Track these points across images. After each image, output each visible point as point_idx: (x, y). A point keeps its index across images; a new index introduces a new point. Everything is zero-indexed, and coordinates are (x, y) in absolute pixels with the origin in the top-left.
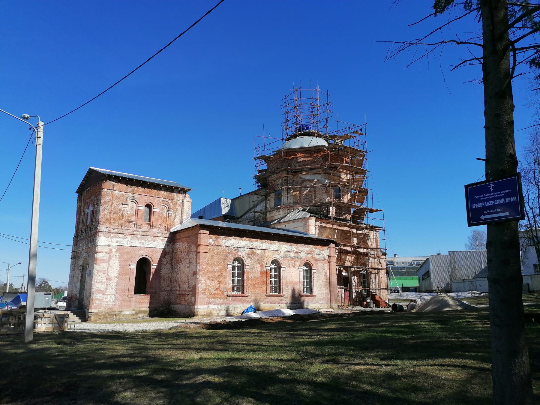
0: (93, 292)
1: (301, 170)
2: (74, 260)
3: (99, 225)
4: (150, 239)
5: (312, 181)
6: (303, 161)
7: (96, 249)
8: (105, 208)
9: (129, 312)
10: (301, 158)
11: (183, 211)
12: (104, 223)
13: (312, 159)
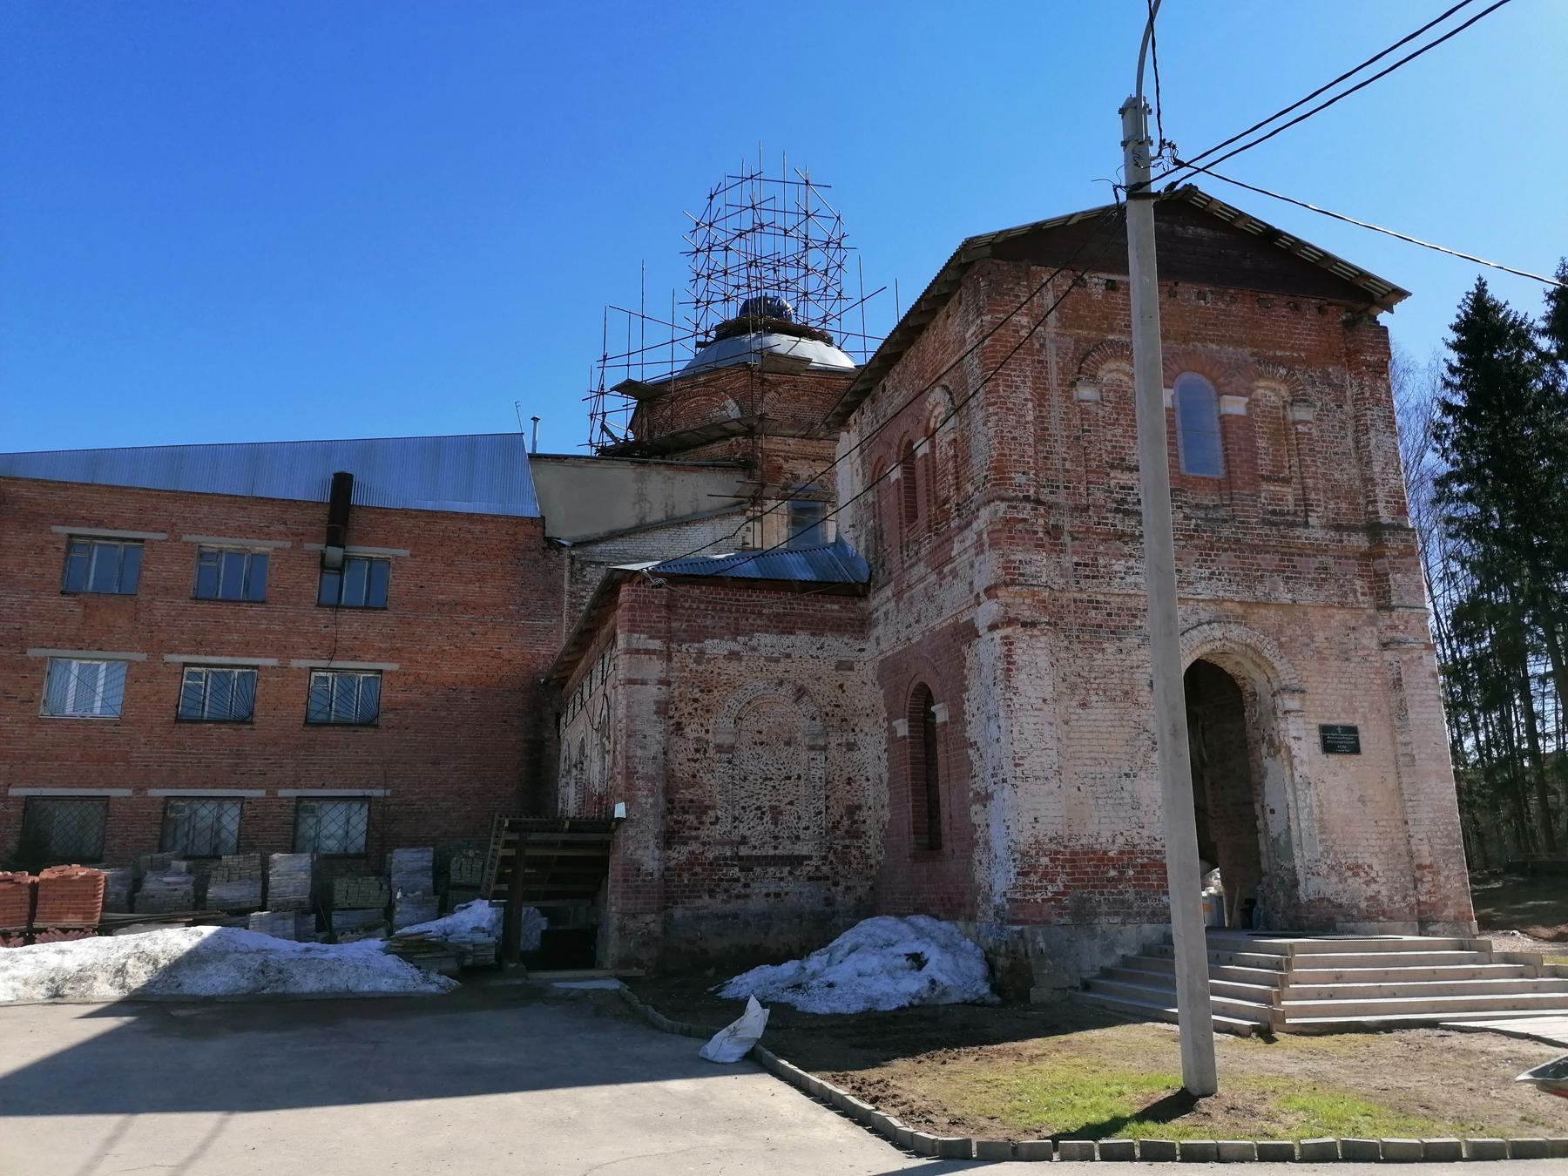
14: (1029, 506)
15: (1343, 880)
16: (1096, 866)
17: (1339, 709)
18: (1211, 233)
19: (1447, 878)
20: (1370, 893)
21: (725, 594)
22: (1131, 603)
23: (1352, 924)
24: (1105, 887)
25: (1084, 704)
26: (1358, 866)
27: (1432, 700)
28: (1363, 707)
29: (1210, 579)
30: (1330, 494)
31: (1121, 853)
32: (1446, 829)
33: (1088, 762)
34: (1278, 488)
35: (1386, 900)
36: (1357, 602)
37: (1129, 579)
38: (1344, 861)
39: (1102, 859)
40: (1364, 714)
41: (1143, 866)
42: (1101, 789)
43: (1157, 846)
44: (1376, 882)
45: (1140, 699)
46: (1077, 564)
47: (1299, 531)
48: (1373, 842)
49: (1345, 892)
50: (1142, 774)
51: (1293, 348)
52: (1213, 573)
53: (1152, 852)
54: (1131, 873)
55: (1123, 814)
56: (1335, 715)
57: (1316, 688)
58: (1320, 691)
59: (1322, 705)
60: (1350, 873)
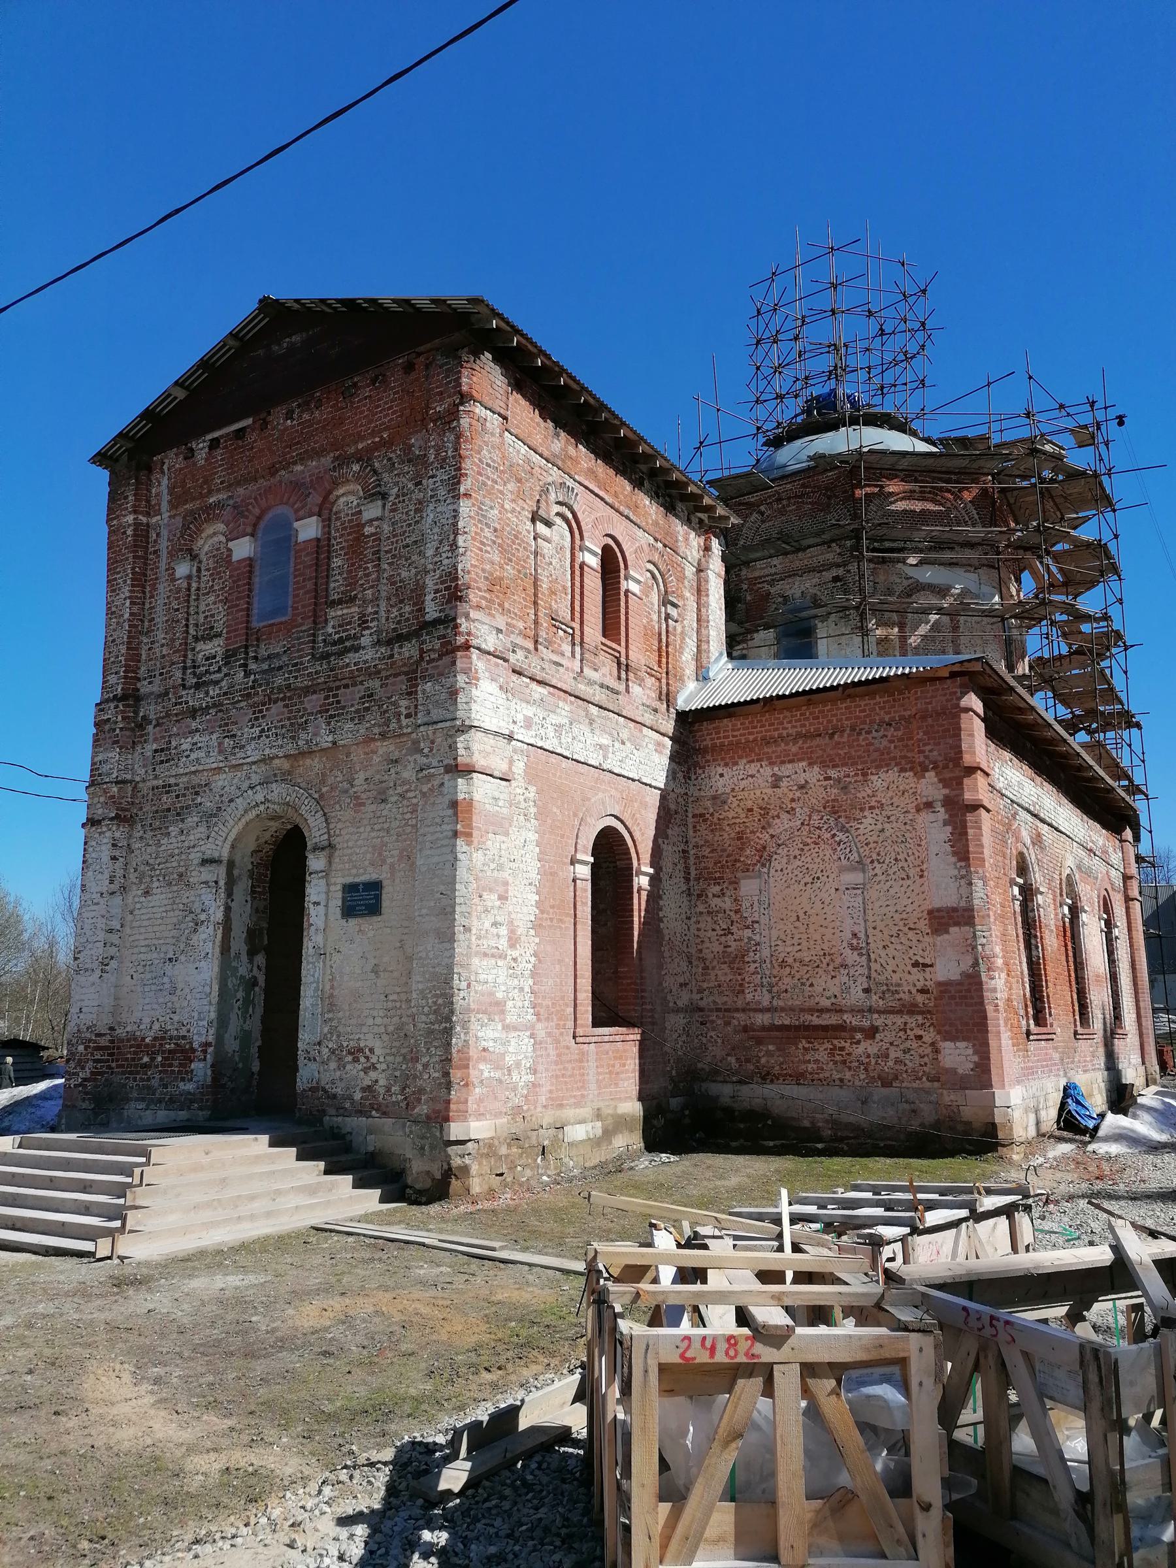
0: (468, 1010)
1: (902, 544)
2: (114, 832)
3: (462, 607)
4: (625, 734)
5: (942, 591)
6: (905, 511)
7: (461, 751)
8: (482, 518)
9: (583, 1125)
10: (897, 501)
11: (704, 617)
12: (484, 603)
13: (937, 508)
14: (112, 705)
15: (342, 1066)
16: (135, 1053)
17: (367, 863)
18: (304, 335)
19: (426, 1066)
20: (367, 1082)
21: (804, 726)
22: (195, 780)
23: (340, 1119)
24: (138, 1072)
25: (147, 892)
26: (361, 1050)
27: (447, 837)
28: (392, 856)
29: (260, 737)
30: (394, 600)
31: (155, 1039)
32: (435, 1003)
33: (143, 950)
34: (345, 611)
35: (382, 1091)
36: (401, 727)
37: (193, 756)
38: (345, 1044)
39: (139, 1045)
40: (392, 866)
41: (170, 1052)
42: (149, 976)
43: (183, 1032)
44: (375, 1068)
45: (191, 880)
46: (156, 751)
47: (351, 658)
48: (378, 1021)
49: (341, 1080)
50: (182, 958)
51: (373, 434)
52: (263, 731)
53: (179, 1037)
54: (160, 1059)
55: (161, 1000)
56: (361, 871)
57: (347, 841)
58: (350, 844)
59: (350, 861)
60: (350, 1058)
